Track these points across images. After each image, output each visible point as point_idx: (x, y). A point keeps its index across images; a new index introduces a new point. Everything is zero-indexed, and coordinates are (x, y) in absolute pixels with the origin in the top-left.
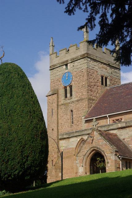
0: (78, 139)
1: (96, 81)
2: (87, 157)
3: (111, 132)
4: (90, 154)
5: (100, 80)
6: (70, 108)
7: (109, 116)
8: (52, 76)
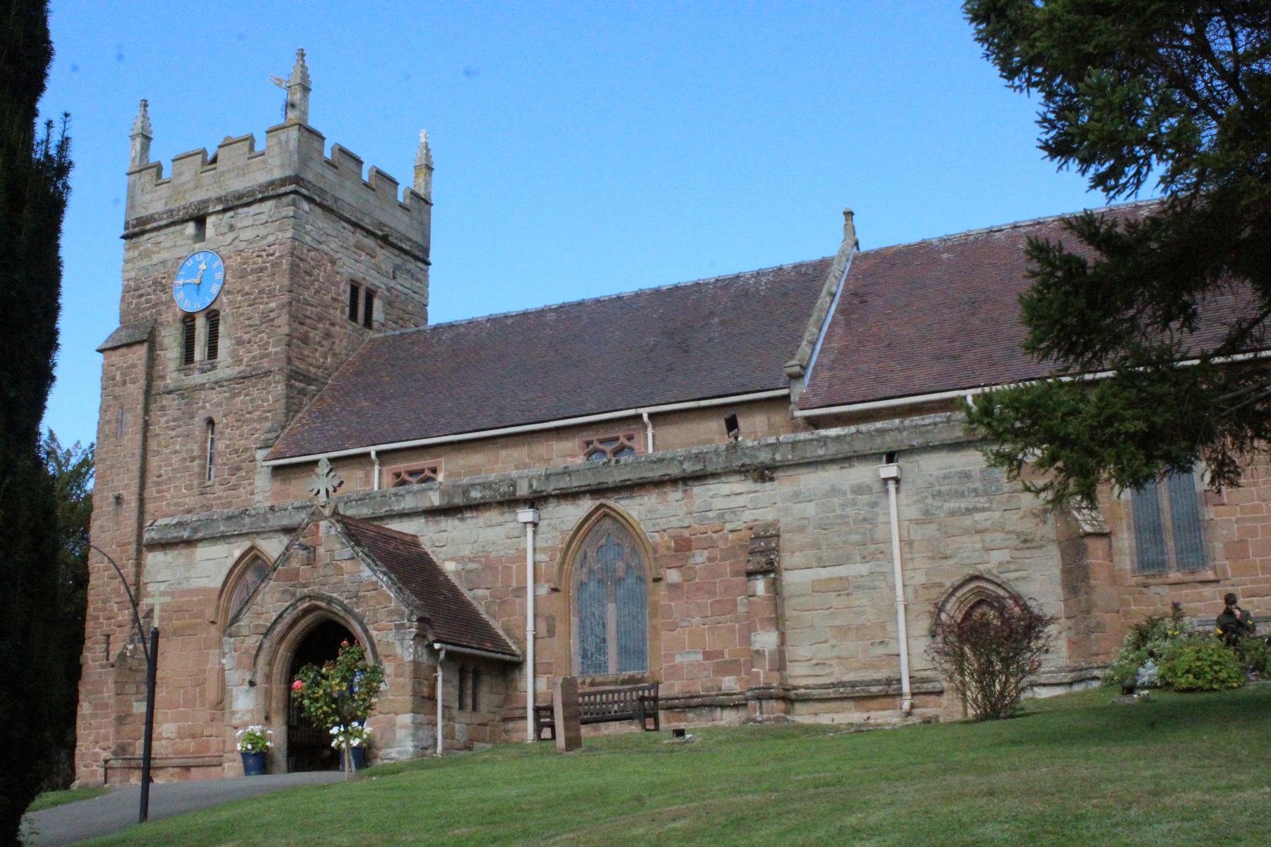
0: (237, 550)
1: (327, 298)
2: (276, 639)
3: (396, 526)
4: (291, 626)
5: (346, 298)
6: (204, 408)
7: (651, 416)
8: (129, 266)
